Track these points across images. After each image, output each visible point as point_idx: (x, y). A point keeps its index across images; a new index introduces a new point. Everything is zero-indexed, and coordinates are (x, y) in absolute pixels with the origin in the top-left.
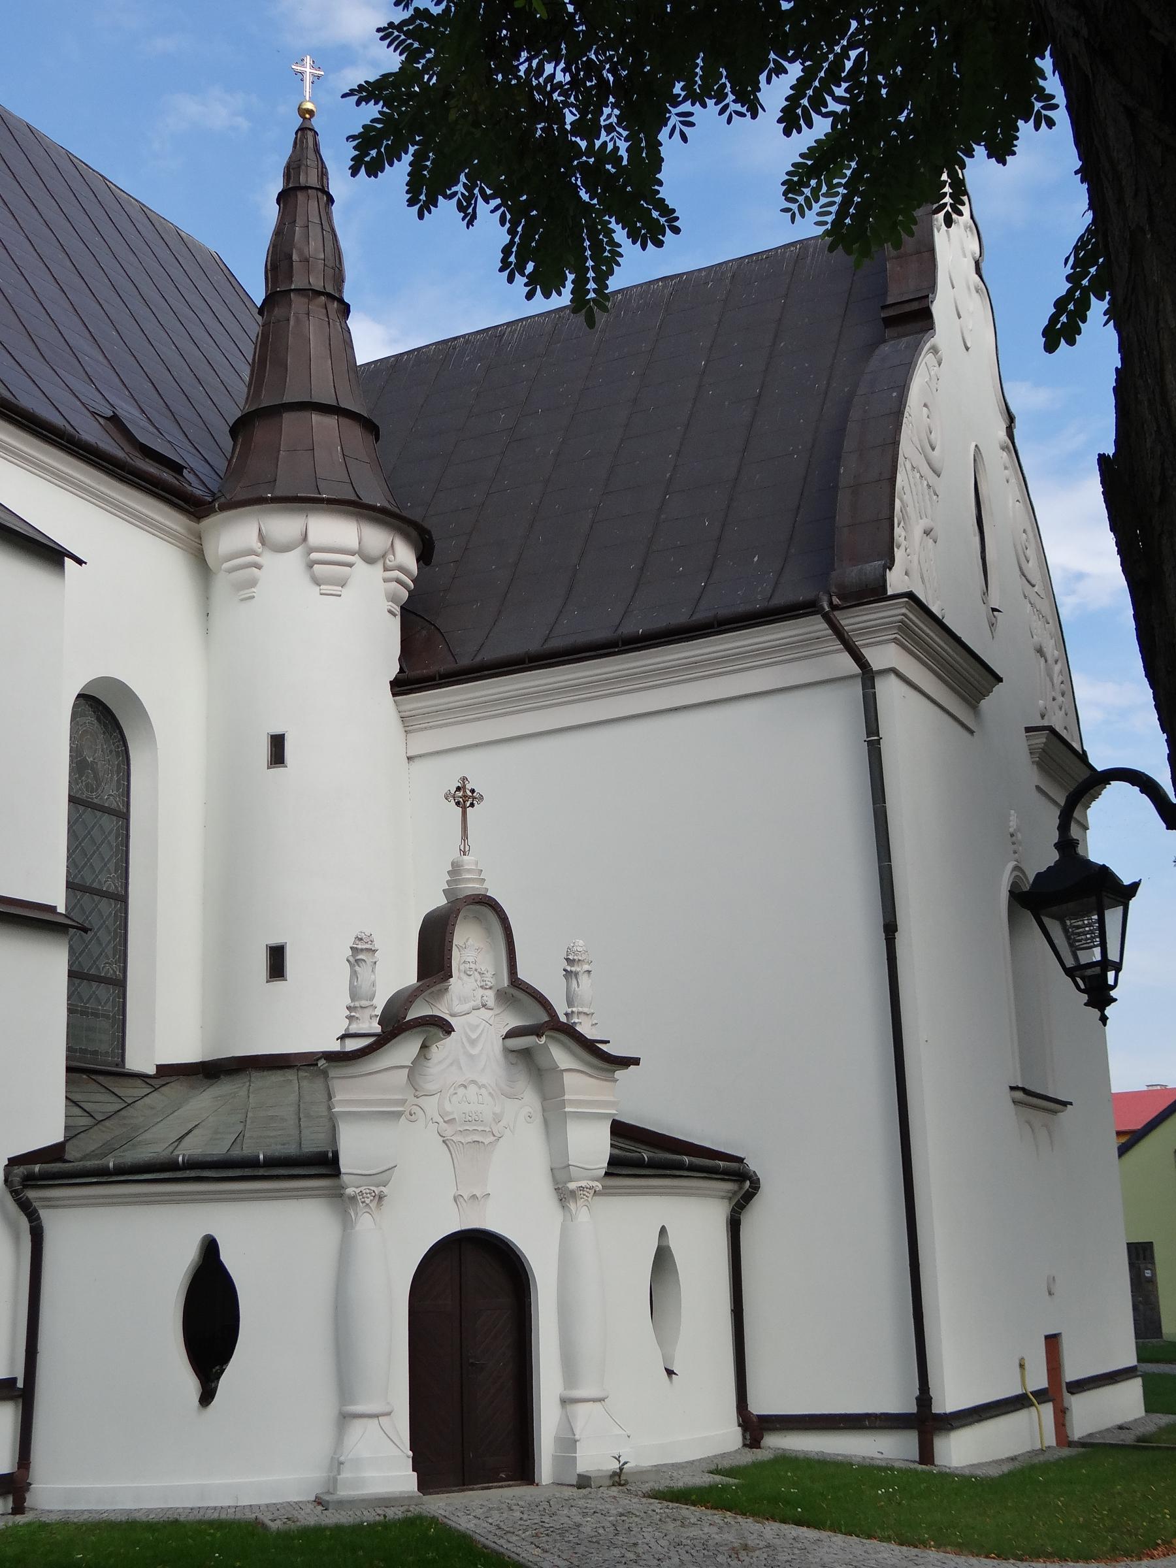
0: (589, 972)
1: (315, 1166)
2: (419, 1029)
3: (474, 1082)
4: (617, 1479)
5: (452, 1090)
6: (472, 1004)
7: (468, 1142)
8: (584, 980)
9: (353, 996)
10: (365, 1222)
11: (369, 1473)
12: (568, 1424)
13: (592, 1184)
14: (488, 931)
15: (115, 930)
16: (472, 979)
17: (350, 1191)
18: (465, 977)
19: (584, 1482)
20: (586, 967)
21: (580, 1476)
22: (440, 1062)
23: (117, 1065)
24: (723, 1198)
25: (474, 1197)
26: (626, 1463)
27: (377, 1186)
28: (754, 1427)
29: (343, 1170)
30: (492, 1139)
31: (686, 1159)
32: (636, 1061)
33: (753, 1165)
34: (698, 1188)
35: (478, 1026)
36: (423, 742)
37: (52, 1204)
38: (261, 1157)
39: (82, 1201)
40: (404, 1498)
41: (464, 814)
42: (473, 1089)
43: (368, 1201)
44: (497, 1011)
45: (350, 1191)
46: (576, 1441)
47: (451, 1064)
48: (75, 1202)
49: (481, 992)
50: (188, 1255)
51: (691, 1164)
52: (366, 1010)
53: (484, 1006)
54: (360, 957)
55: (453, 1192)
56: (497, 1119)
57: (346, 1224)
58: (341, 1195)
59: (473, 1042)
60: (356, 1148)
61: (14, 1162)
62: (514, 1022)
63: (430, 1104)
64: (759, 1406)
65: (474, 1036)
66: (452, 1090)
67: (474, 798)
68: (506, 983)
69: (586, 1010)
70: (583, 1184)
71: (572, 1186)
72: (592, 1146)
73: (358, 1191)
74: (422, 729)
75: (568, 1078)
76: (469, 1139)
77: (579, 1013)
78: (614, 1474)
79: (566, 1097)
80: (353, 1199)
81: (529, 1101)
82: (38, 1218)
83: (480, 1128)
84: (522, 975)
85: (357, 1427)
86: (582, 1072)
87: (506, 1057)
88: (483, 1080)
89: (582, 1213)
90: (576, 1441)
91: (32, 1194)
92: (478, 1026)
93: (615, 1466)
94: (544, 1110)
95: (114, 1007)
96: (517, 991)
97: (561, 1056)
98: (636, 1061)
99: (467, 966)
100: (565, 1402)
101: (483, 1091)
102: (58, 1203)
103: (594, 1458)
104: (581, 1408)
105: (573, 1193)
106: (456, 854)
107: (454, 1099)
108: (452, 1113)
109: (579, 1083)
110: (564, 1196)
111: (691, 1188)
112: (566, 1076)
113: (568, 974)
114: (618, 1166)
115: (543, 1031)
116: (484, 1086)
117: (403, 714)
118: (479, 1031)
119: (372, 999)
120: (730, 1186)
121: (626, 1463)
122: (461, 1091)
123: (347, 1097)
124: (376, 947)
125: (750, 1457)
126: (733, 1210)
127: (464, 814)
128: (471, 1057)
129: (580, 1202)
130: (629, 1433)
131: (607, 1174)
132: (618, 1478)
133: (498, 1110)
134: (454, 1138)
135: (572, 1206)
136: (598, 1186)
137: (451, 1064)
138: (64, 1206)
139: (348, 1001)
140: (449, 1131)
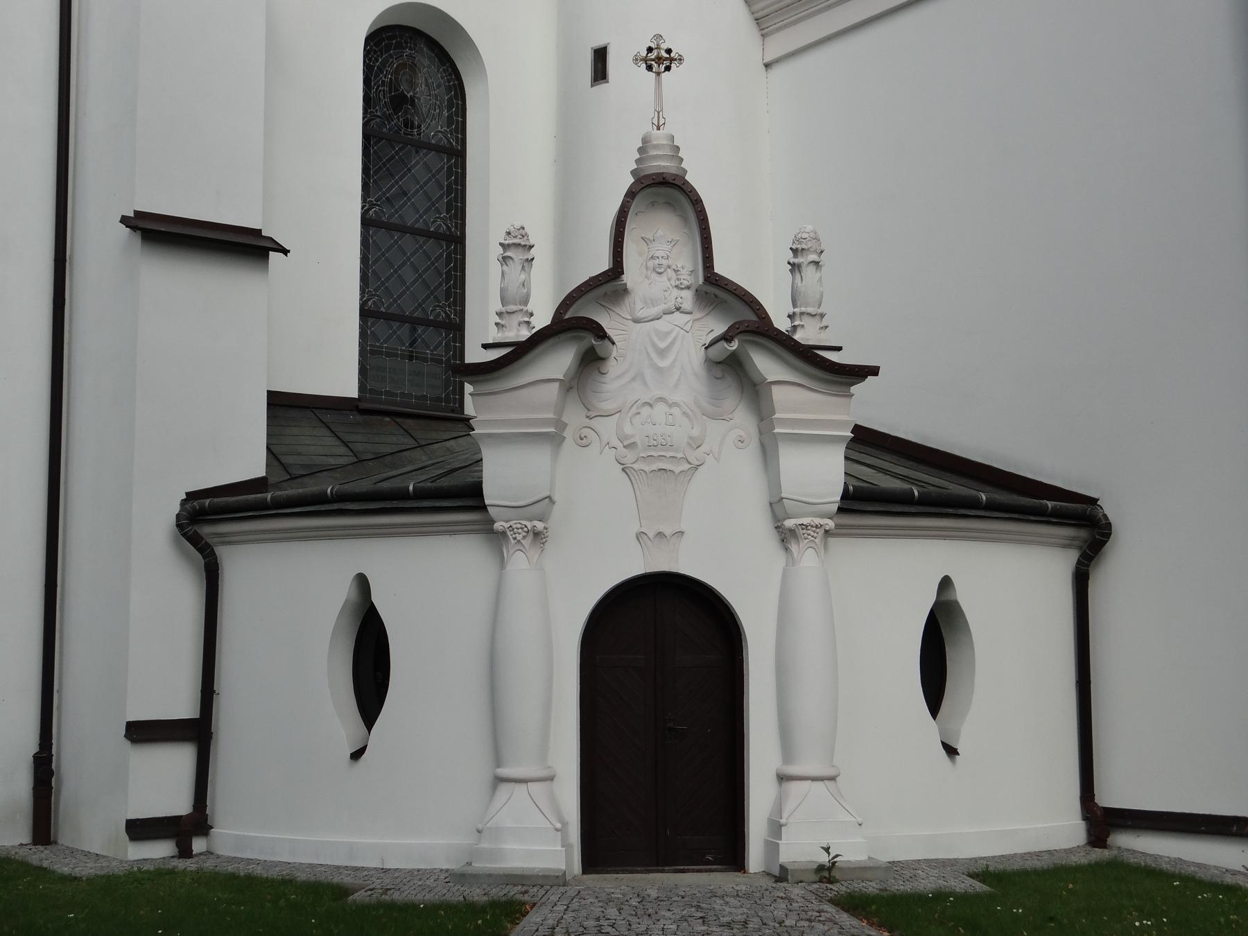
0: (817, 263)
1: (457, 498)
2: (570, 334)
3: (661, 399)
4: (826, 874)
5: (634, 410)
6: (662, 307)
7: (659, 470)
8: (809, 272)
9: (504, 301)
10: (520, 561)
11: (510, 846)
12: (779, 807)
13: (817, 521)
14: (685, 219)
15: (448, 273)
16: (664, 278)
17: (498, 526)
18: (654, 275)
19: (783, 875)
20: (813, 257)
21: (783, 868)
22: (618, 377)
23: (453, 411)
24: (1065, 546)
25: (660, 535)
26: (837, 856)
27: (531, 521)
28: (1102, 822)
29: (487, 502)
30: (687, 466)
31: (1050, 504)
32: (874, 371)
33: (1110, 508)
34: (1008, 532)
35: (668, 333)
36: (780, 44)
37: (228, 540)
38: (411, 488)
39: (266, 536)
40: (538, 876)
41: (659, 83)
42: (661, 408)
43: (519, 537)
44: (698, 315)
45: (498, 526)
46: (781, 826)
47: (634, 379)
48: (251, 537)
49: (676, 292)
50: (341, 593)
51: (1054, 508)
52: (514, 316)
53: (678, 309)
54: (508, 254)
55: (636, 528)
56: (696, 444)
57: (502, 563)
58: (491, 531)
59: (662, 353)
60: (505, 475)
61: (191, 496)
62: (720, 328)
63: (607, 427)
64: (1111, 796)
65: (662, 345)
66: (634, 410)
67: (672, 60)
68: (701, 280)
69: (810, 310)
70: (805, 521)
71: (789, 523)
72: (821, 473)
73: (507, 525)
74: (778, 30)
75: (778, 393)
76: (655, 467)
77: (802, 314)
78: (821, 868)
79: (777, 416)
80: (504, 533)
81: (742, 420)
82: (213, 553)
83: (669, 454)
84: (720, 268)
85: (504, 789)
86: (799, 385)
87: (709, 370)
88: (676, 397)
89: (808, 557)
90: (781, 826)
91: (206, 530)
92: (668, 333)
93: (824, 859)
94: (761, 433)
95: (447, 352)
96: (716, 290)
97: (766, 365)
98: (874, 371)
99: (657, 262)
100: (782, 778)
101: (675, 410)
102: (227, 539)
103: (801, 848)
104: (794, 787)
105: (792, 532)
106: (648, 128)
107: (637, 420)
108: (632, 436)
109: (795, 398)
110: (786, 536)
111: (969, 530)
112: (776, 390)
113: (795, 268)
114: (857, 501)
115: (746, 337)
116: (676, 404)
117: (757, 15)
118: (669, 340)
119: (526, 302)
120: (1083, 534)
121: (837, 856)
122: (646, 411)
123: (490, 417)
124: (532, 243)
125: (1098, 854)
126: (1079, 562)
127: (659, 83)
128: (660, 370)
129: (804, 543)
130: (860, 820)
131: (841, 510)
132: (826, 873)
133: (695, 432)
134: (635, 466)
135: (794, 547)
136: (830, 524)
137: (634, 379)
138: (230, 543)
139: (498, 306)
140: (629, 457)
